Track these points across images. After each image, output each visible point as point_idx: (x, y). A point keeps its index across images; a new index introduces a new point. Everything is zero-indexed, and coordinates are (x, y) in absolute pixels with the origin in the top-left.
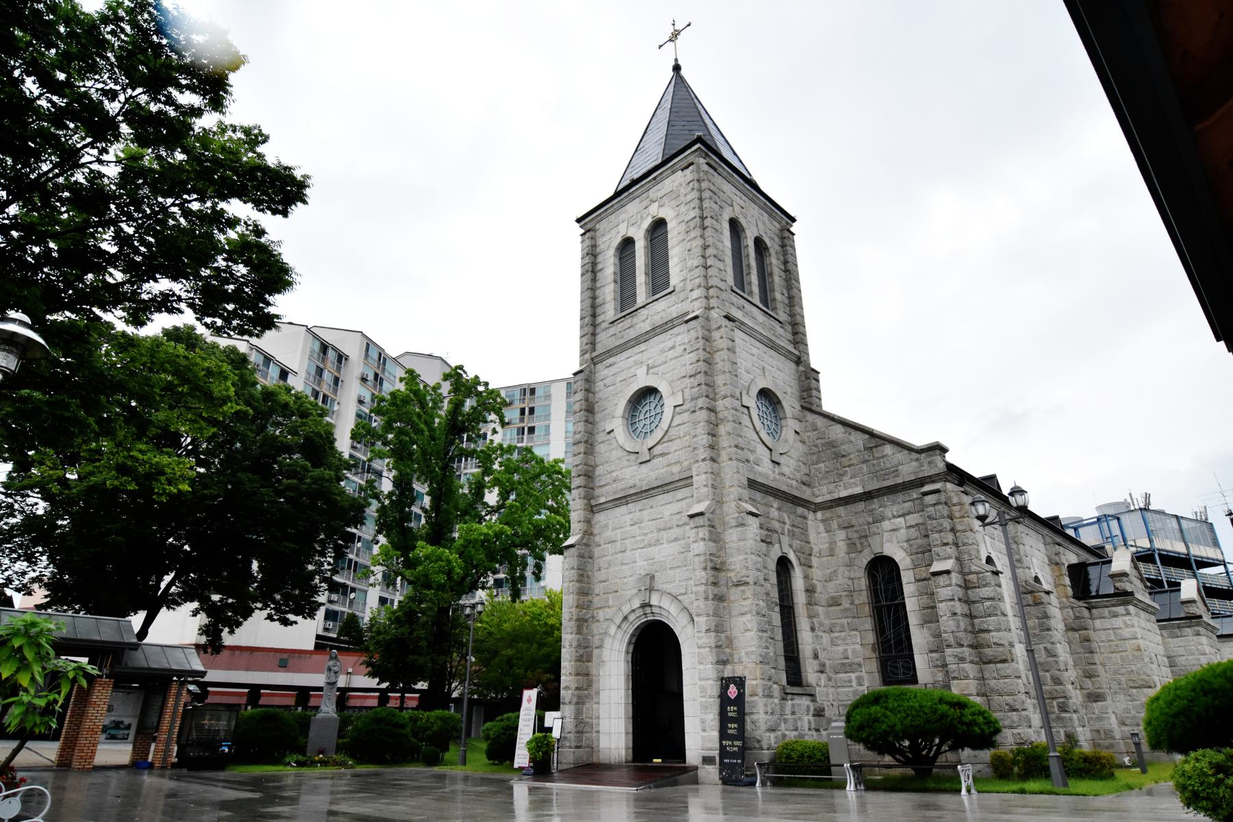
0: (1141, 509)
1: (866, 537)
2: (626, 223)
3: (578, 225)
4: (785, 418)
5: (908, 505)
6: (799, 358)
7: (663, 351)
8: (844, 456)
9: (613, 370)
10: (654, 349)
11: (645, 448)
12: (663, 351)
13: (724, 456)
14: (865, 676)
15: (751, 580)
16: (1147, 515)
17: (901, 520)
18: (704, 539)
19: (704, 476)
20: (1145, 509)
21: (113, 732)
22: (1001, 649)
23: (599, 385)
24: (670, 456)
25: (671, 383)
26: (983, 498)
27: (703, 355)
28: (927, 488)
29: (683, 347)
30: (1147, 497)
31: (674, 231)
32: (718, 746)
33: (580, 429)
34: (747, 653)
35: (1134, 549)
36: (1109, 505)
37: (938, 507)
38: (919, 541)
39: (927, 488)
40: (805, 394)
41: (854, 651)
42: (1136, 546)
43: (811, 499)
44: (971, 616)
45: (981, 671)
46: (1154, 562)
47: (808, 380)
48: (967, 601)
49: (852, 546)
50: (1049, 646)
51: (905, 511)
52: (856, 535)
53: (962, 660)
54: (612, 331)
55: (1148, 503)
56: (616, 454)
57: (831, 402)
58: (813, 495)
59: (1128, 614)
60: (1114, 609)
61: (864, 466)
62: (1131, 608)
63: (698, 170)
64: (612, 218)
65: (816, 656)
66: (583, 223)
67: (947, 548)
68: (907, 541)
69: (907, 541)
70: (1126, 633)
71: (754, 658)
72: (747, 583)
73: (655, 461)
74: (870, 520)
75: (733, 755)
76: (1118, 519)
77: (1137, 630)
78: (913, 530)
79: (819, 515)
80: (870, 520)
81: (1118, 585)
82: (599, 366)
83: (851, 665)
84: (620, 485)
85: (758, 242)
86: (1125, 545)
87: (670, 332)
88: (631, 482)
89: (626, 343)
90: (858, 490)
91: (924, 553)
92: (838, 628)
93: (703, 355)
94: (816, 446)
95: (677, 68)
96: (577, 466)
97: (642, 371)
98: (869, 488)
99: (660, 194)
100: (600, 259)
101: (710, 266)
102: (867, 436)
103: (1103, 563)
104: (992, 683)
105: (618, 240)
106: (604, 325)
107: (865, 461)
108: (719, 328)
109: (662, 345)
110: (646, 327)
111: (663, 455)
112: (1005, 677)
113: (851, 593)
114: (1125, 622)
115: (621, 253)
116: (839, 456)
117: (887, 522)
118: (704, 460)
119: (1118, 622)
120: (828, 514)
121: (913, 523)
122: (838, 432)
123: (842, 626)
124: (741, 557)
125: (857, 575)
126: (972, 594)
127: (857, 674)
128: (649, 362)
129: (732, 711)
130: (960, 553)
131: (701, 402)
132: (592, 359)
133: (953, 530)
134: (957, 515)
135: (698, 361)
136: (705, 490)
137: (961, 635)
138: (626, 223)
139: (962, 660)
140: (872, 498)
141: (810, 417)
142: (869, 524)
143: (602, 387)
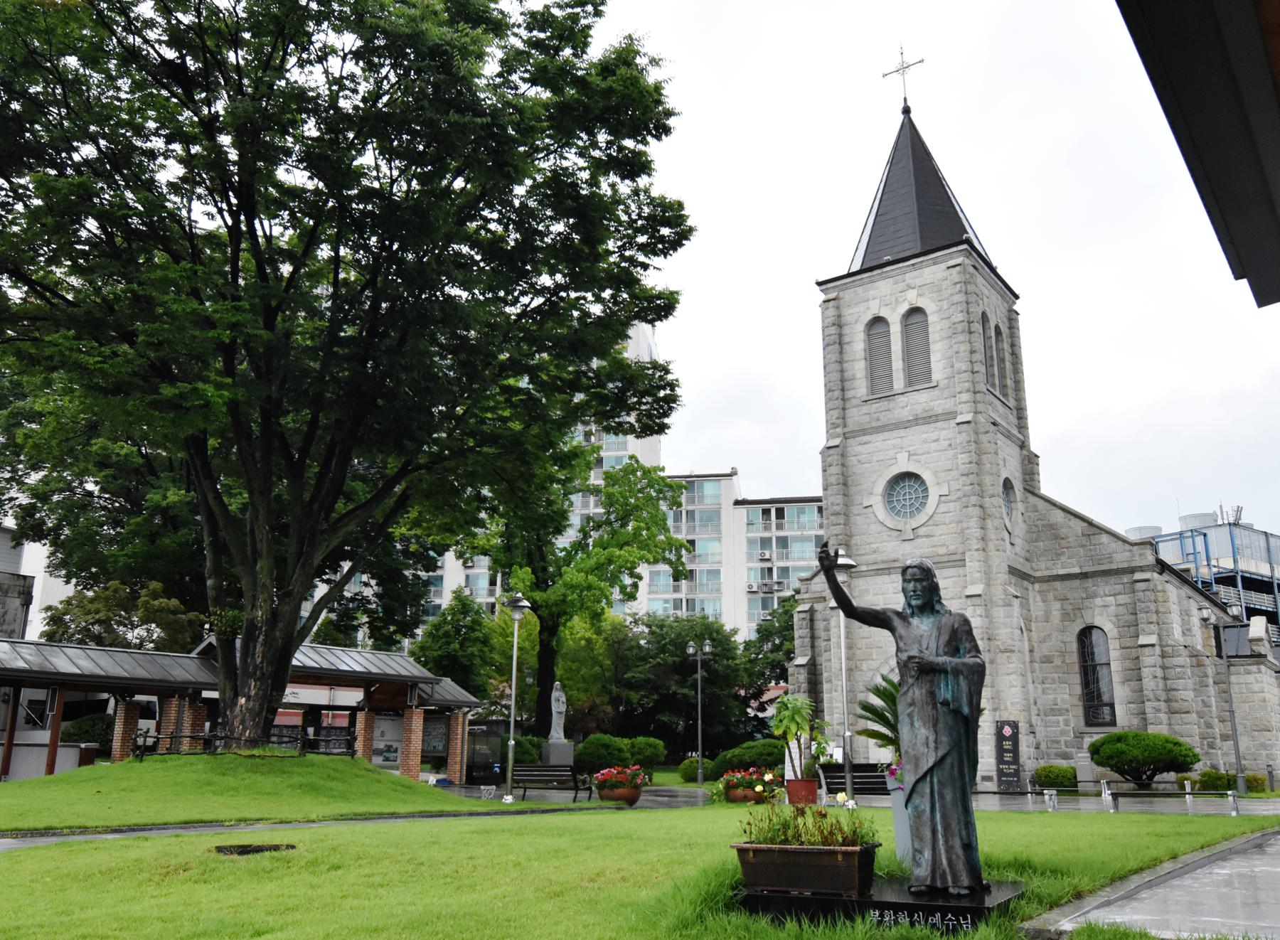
0: (1230, 524)
1: (1080, 609)
2: (878, 301)
3: (817, 288)
4: (1016, 502)
5: (1119, 588)
6: (1023, 443)
7: (925, 442)
8: (1063, 538)
9: (868, 448)
10: (916, 437)
11: (909, 528)
12: (925, 442)
13: (991, 546)
14: (1072, 719)
15: (1016, 649)
16: (1237, 531)
17: (1112, 598)
18: (981, 616)
19: (977, 563)
20: (1235, 524)
21: (387, 755)
22: (1186, 703)
23: (852, 460)
24: (935, 538)
25: (935, 473)
26: (1207, 606)
27: (975, 459)
28: (1138, 576)
29: (948, 442)
30: (1239, 510)
31: (936, 325)
32: (995, 768)
33: (838, 501)
34: (1012, 703)
35: (1215, 570)
36: (1195, 516)
37: (1147, 593)
38: (1127, 617)
39: (1138, 576)
40: (1028, 477)
41: (1063, 700)
42: (1218, 567)
43: (1030, 572)
44: (1165, 679)
45: (1169, 719)
46: (1235, 586)
47: (1030, 462)
48: (1164, 668)
49: (1066, 616)
50: (1205, 698)
51: (1117, 592)
52: (1070, 607)
53: (1159, 711)
54: (865, 409)
55: (1238, 518)
56: (874, 528)
57: (1048, 487)
58: (1032, 568)
59: (1260, 672)
60: (1248, 667)
61: (1081, 550)
62: (1262, 667)
63: (964, 272)
64: (859, 290)
65: (1035, 703)
66: (824, 287)
67: (1152, 626)
68: (1116, 616)
69: (1116, 616)
70: (1256, 687)
71: (1018, 707)
72: (1012, 651)
73: (919, 541)
74: (1084, 596)
75: (1009, 775)
76: (1205, 535)
77: (1265, 685)
78: (1121, 608)
79: (1037, 586)
80: (1084, 596)
81: (1254, 648)
82: (851, 441)
83: (1059, 710)
84: (879, 557)
85: (997, 328)
86: (1208, 565)
87: (933, 425)
88: (893, 556)
89: (884, 426)
90: (1076, 570)
91: (1131, 627)
92: (1049, 681)
93: (975, 459)
94: (1036, 526)
95: (906, 111)
96: (837, 535)
97: (903, 457)
98: (1086, 569)
99: (918, 282)
100: (846, 330)
101: (977, 372)
102: (1086, 524)
103: (1242, 626)
104: (1177, 728)
105: (869, 317)
106: (855, 402)
107: (1083, 546)
108: (987, 432)
109: (925, 436)
110: (906, 414)
111: (927, 536)
112: (1188, 723)
113: (1063, 654)
114: (1256, 678)
115: (869, 330)
116: (1057, 537)
117: (1099, 599)
118: (977, 550)
119: (1250, 678)
120: (1045, 586)
121: (1122, 602)
122: (1058, 516)
123: (1053, 679)
124: (1007, 631)
125: (1069, 639)
126: (1168, 662)
127: (1065, 717)
128: (910, 449)
129: (1007, 745)
130: (1160, 629)
131: (974, 499)
132: (844, 434)
133: (1157, 612)
134: (1160, 599)
135: (970, 463)
136: (978, 575)
137: (1159, 692)
138: (878, 301)
139: (1159, 711)
140: (1087, 577)
141: (1032, 499)
142: (1082, 599)
143: (856, 463)
